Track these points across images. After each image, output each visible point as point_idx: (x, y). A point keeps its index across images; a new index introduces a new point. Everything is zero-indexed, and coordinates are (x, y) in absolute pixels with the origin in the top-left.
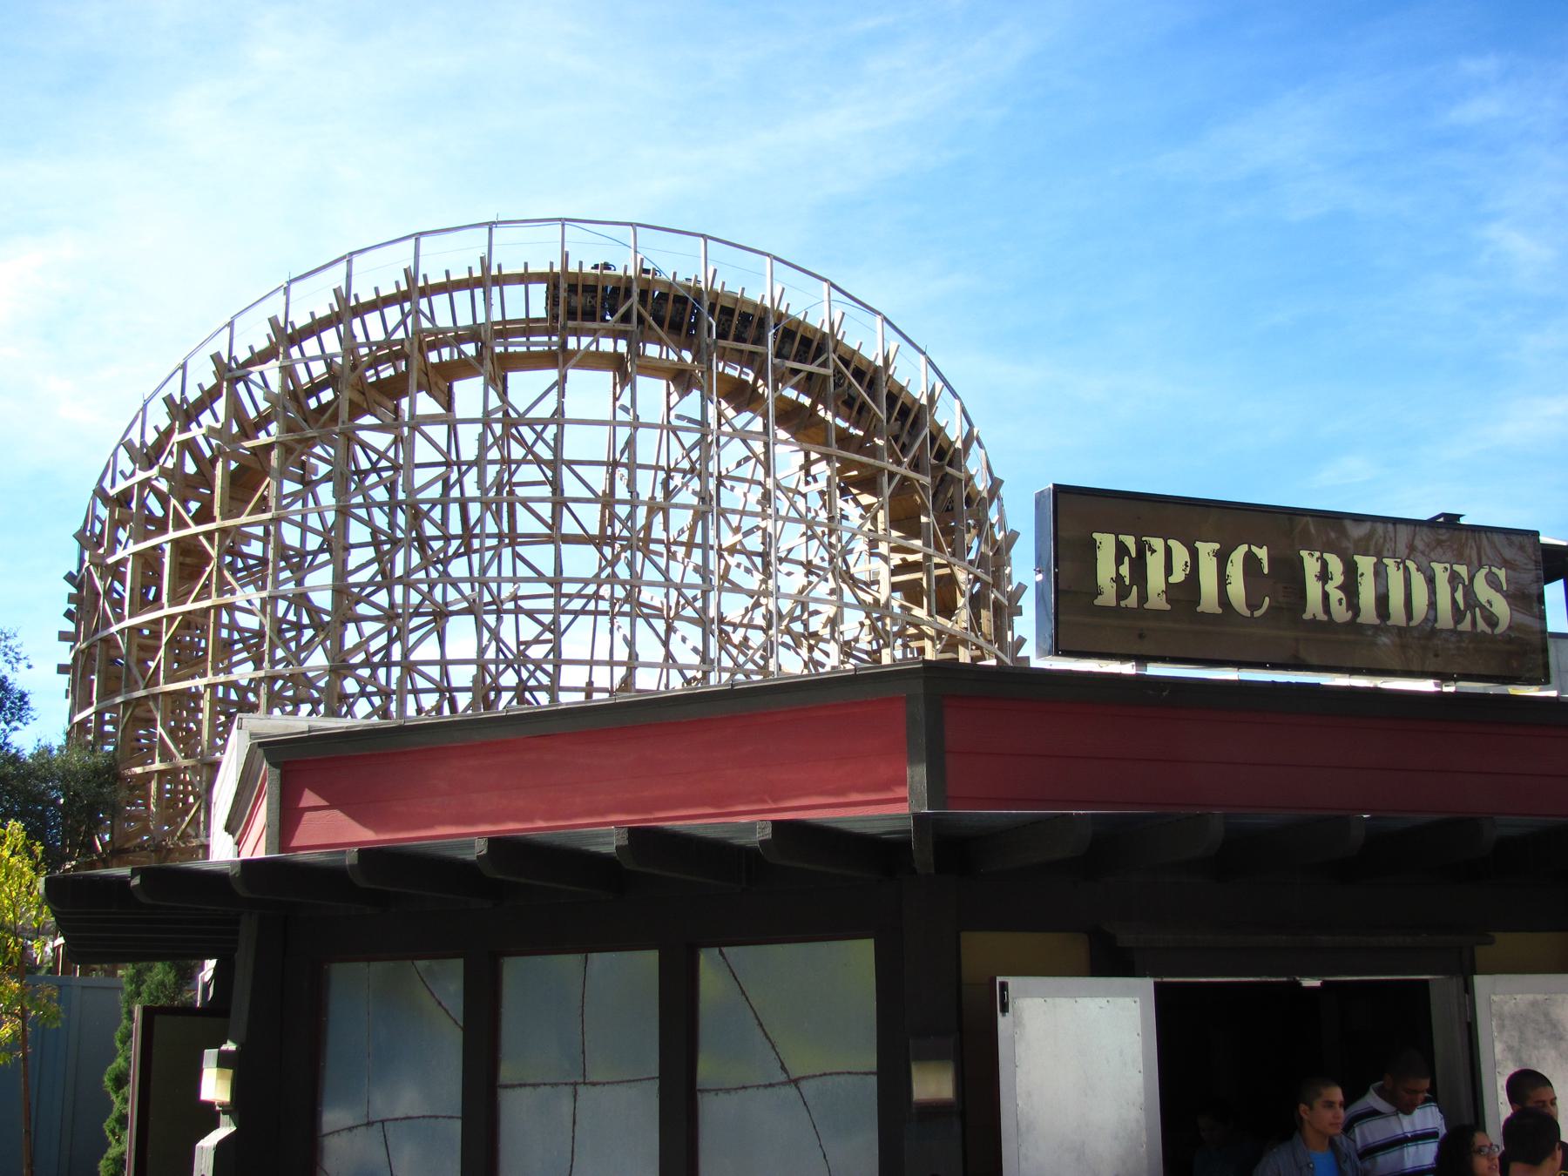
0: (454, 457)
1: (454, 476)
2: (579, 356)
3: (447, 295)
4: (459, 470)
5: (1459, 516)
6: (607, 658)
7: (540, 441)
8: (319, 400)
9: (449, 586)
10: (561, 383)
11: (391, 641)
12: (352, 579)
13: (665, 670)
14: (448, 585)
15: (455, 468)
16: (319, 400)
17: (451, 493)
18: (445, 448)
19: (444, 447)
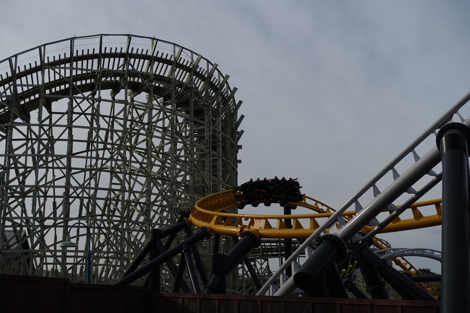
0: (29, 137)
1: (30, 144)
2: (111, 75)
3: (64, 185)
4: (32, 142)
5: (430, 270)
6: (55, 170)
7: (80, 234)
8: (81, 83)
9: (50, 69)
10: (103, 116)
11: (27, 149)
12: (16, 153)
13: (76, 258)
14: (50, 69)
15: (30, 141)
16: (81, 83)
17: (24, 170)
18: (26, 134)
19: (26, 134)
